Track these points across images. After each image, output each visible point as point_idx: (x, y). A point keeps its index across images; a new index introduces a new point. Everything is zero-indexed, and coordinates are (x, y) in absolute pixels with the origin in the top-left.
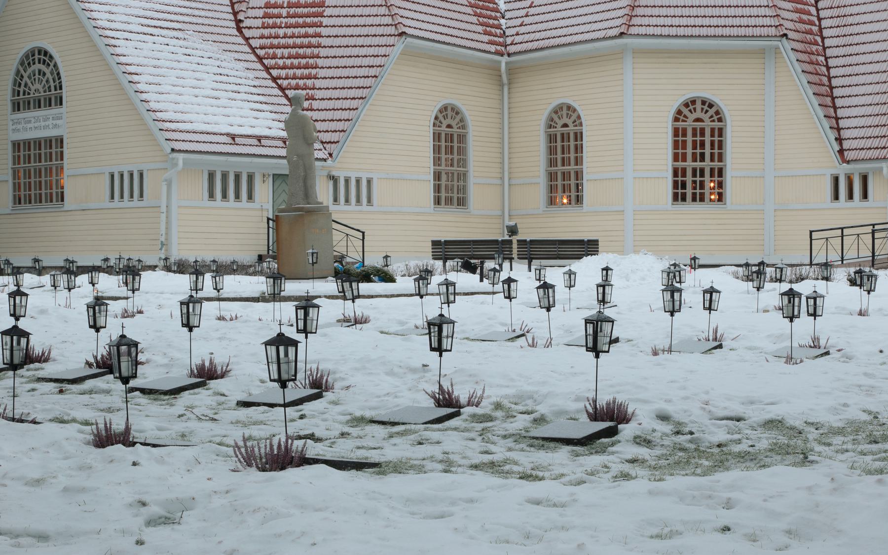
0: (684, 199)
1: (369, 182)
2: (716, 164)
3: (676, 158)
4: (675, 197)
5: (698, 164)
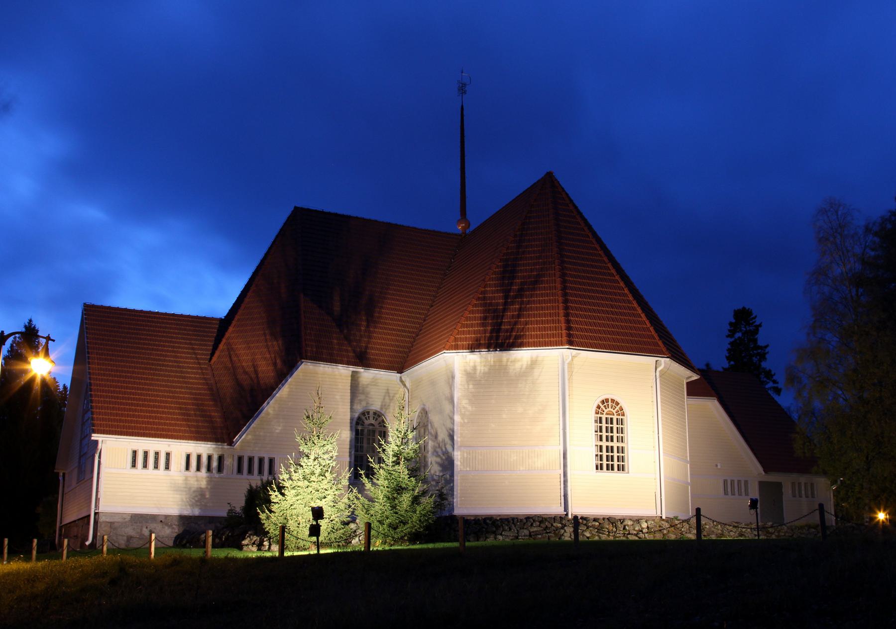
2: (620, 445)
5: (610, 444)
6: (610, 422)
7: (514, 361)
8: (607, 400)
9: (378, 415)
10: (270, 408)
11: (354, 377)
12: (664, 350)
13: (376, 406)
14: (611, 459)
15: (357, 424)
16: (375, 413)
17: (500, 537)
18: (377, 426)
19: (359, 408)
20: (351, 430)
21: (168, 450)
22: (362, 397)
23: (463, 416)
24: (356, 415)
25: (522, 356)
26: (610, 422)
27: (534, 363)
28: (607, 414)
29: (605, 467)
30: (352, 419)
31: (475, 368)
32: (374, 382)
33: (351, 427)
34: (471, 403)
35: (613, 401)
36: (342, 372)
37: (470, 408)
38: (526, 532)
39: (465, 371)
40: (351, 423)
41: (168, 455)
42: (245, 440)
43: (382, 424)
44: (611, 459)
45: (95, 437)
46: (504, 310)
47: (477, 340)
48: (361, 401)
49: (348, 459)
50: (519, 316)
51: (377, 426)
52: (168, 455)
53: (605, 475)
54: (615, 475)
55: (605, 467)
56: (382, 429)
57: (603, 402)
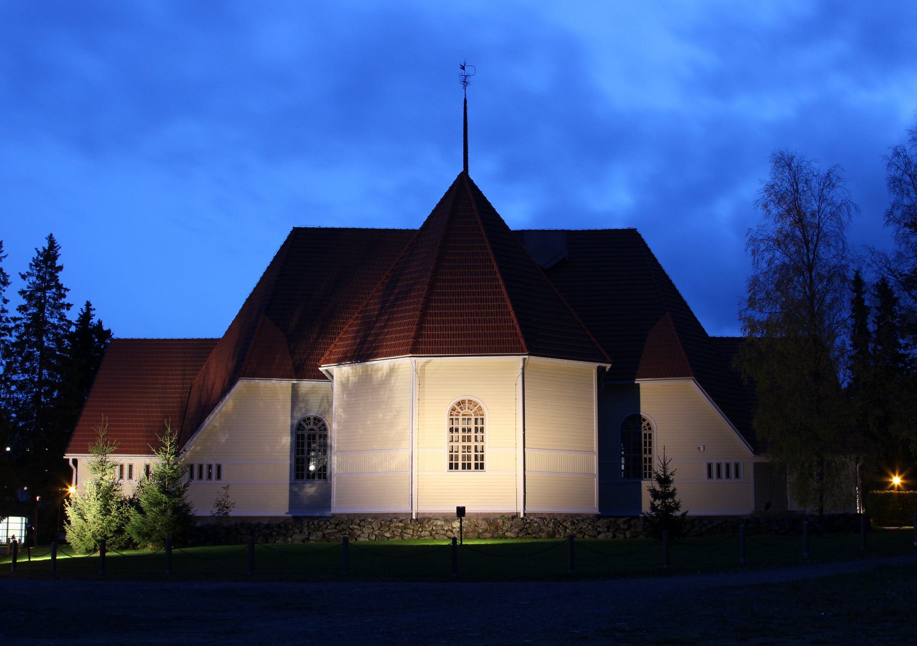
0: (457, 468)
1: (737, 465)
3: (298, 454)
4: (451, 467)
6: (467, 424)
7: (377, 370)
8: (463, 402)
9: (317, 420)
10: (214, 420)
11: (294, 388)
12: (524, 346)
13: (313, 413)
14: (467, 460)
15: (298, 429)
16: (315, 419)
17: (290, 539)
18: (317, 430)
19: (299, 415)
20: (292, 435)
21: (130, 462)
22: (302, 405)
23: (339, 423)
24: (296, 422)
25: (382, 365)
26: (467, 424)
27: (392, 370)
28: (464, 415)
29: (473, 466)
30: (292, 426)
31: (348, 379)
32: (313, 390)
33: (292, 433)
34: (345, 411)
35: (470, 401)
36: (282, 386)
37: (344, 416)
38: (320, 534)
39: (341, 382)
40: (292, 429)
41: (131, 467)
42: (193, 447)
43: (324, 428)
44: (467, 460)
45: (70, 457)
46: (375, 322)
47: (346, 353)
48: (300, 409)
49: (289, 462)
50: (384, 327)
51: (317, 430)
52: (131, 467)
53: (461, 475)
54: (472, 475)
55: (473, 466)
56: (323, 433)
57: (459, 404)
